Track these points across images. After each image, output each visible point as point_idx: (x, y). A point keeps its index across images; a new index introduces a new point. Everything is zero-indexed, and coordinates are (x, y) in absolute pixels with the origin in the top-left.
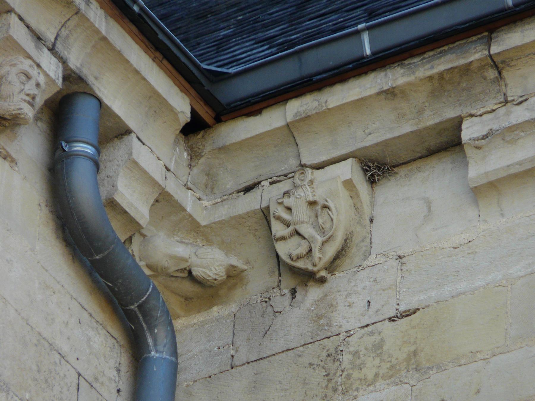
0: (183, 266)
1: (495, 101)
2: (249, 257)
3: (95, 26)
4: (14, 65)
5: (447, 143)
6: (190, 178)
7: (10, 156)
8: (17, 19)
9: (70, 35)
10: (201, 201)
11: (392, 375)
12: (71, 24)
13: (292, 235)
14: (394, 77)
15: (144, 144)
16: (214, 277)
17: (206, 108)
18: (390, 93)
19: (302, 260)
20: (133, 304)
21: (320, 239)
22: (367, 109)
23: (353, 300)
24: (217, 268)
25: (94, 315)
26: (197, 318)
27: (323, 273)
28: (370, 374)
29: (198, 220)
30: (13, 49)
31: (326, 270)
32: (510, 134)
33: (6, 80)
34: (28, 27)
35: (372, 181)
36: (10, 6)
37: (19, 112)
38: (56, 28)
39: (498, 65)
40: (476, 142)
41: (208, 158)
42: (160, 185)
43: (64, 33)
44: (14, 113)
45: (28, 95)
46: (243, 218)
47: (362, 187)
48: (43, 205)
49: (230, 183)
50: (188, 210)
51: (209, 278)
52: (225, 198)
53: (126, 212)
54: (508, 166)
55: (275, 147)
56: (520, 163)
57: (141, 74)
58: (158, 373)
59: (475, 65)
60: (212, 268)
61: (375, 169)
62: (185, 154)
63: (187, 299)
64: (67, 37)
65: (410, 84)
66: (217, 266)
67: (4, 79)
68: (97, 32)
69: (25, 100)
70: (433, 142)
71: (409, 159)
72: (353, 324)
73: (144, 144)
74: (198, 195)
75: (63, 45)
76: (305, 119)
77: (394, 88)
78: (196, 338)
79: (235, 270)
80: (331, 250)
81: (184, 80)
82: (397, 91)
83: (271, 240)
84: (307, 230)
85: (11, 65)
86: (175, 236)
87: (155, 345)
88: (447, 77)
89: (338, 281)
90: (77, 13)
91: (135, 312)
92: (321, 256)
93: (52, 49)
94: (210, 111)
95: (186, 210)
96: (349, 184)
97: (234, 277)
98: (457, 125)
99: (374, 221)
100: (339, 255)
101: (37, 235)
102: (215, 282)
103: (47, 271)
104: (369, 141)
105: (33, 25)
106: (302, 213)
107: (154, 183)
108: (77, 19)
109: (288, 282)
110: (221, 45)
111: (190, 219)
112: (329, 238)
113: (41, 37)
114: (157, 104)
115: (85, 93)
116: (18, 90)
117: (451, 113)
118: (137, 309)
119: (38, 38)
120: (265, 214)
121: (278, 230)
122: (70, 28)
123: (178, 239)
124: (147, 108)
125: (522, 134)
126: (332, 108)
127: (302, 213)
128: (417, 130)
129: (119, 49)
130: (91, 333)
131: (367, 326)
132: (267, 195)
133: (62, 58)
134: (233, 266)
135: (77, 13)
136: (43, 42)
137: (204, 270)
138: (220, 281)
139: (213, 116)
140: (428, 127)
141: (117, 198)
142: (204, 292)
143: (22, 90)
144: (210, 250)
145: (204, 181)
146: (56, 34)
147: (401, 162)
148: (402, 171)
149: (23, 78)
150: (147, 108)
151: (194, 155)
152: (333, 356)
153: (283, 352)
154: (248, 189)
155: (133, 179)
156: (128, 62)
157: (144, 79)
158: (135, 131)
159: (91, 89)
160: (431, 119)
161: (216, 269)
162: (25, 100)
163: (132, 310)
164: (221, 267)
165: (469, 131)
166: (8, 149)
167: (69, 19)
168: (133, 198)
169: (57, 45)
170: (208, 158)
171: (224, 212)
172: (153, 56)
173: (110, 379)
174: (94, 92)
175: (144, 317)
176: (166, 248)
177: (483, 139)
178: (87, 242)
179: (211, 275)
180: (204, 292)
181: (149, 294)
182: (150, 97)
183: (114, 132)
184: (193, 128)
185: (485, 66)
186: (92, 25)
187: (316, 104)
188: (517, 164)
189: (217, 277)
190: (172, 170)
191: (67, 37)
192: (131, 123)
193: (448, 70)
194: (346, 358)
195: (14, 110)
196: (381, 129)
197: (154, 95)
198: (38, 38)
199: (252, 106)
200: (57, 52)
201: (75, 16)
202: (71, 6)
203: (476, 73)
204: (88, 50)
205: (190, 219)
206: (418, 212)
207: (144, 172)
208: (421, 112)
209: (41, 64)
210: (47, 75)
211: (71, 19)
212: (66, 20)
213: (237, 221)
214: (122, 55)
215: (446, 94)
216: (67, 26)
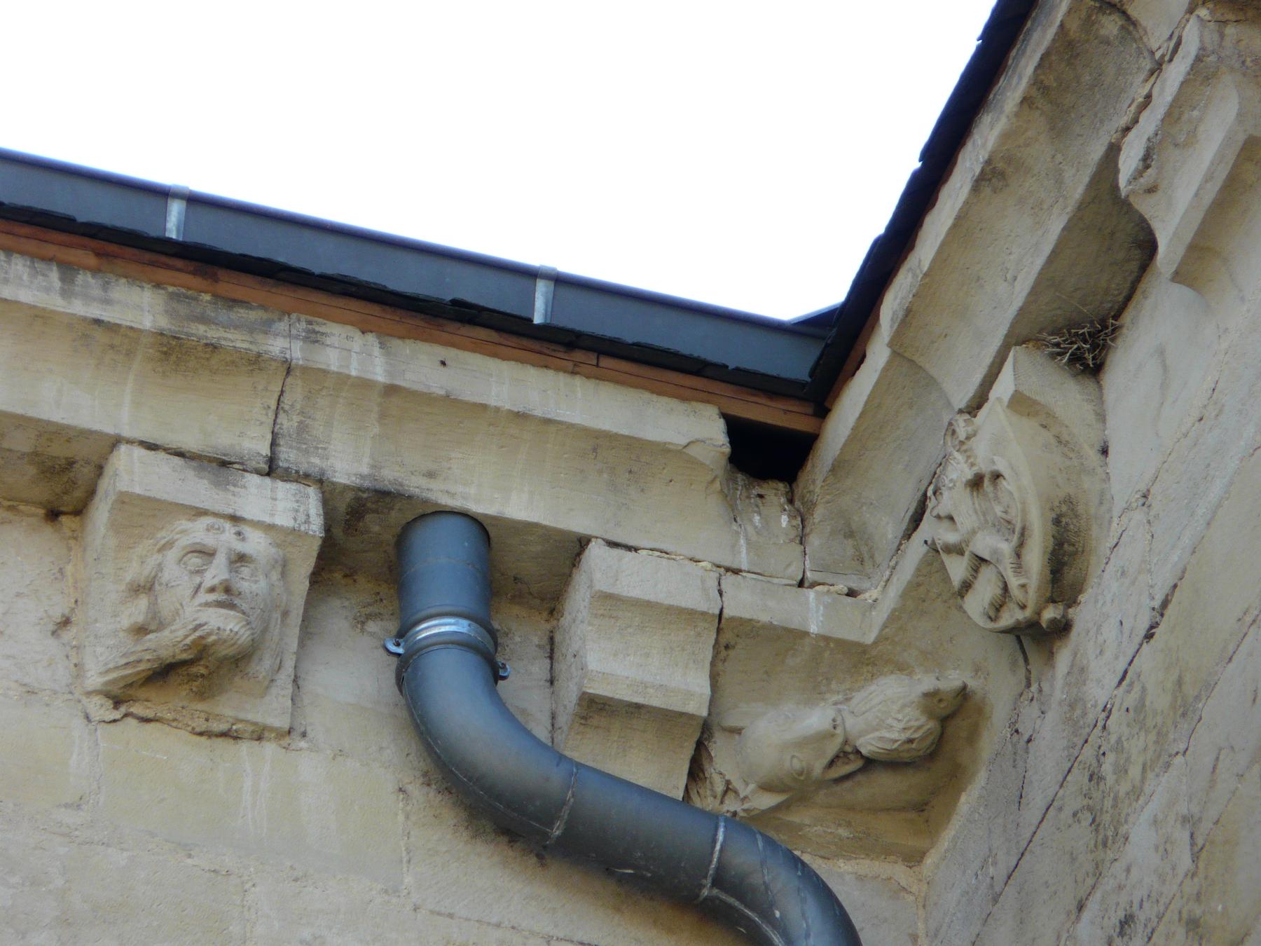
0: (832, 749)
1: (1142, 76)
3: (349, 377)
4: (169, 545)
6: (807, 562)
7: (265, 728)
8: (139, 452)
9: (308, 421)
10: (861, 597)
12: (295, 395)
13: (976, 570)
15: (636, 550)
16: (904, 737)
18: (990, 177)
19: (1005, 608)
20: (701, 887)
21: (1006, 548)
24: (900, 716)
27: (1050, 613)
30: (154, 516)
31: (1054, 602)
33: (161, 584)
34: (180, 454)
37: (198, 634)
38: (262, 423)
40: (1142, 180)
41: (828, 502)
42: (703, 614)
43: (288, 423)
44: (188, 641)
45: (212, 590)
46: (919, 585)
49: (888, 527)
50: (814, 629)
51: (896, 745)
52: (892, 563)
53: (638, 707)
54: (1196, 195)
55: (911, 407)
56: (1209, 178)
57: (534, 417)
59: (1074, 26)
60: (890, 721)
61: (1072, 343)
63: (921, 807)
64: (302, 428)
65: (1006, 136)
66: (899, 712)
67: (156, 585)
68: (364, 384)
69: (207, 604)
71: (1128, 285)
73: (636, 550)
75: (298, 449)
77: (989, 162)
79: (940, 701)
80: (1035, 558)
81: (681, 375)
82: (1000, 165)
84: (985, 543)
85: (159, 551)
86: (828, 696)
88: (1050, 80)
90: (289, 371)
91: (718, 898)
92: (1023, 581)
93: (272, 469)
94: (793, 406)
95: (806, 634)
97: (954, 716)
99: (1111, 451)
101: (404, 854)
102: (914, 746)
103: (451, 916)
105: (190, 442)
107: (689, 616)
108: (299, 382)
111: (832, 645)
112: (1022, 534)
113: (226, 458)
114: (625, 458)
115: (423, 516)
116: (189, 592)
118: (715, 891)
119: (221, 465)
122: (298, 406)
123: (835, 698)
124: (605, 476)
125: (1195, 113)
126: (930, 269)
128: (1070, 220)
129: (442, 392)
131: (1126, 672)
133: (307, 476)
134: (927, 695)
135: (289, 371)
136: (237, 466)
137: (877, 734)
138: (923, 738)
139: (810, 410)
140: (1081, 203)
143: (200, 586)
144: (873, 688)
145: (850, 551)
146: (269, 437)
147: (1121, 298)
148: (1127, 317)
149: (195, 561)
150: (605, 476)
155: (630, 630)
157: (548, 421)
158: (594, 534)
159: (426, 502)
161: (899, 721)
162: (207, 604)
163: (706, 899)
164: (907, 710)
166: (250, 717)
167: (282, 392)
169: (282, 456)
170: (828, 502)
172: (570, 365)
174: (437, 504)
175: (741, 899)
177: (1147, 167)
179: (895, 736)
181: (721, 850)
182: (595, 450)
183: (522, 579)
185: (1089, 16)
186: (343, 380)
187: (909, 279)
188: (1206, 181)
189: (908, 735)
190: (744, 566)
191: (302, 428)
192: (578, 524)
193: (1036, 69)
195: (186, 636)
197: (599, 444)
198: (221, 465)
200: (287, 469)
201: (289, 380)
202: (263, 365)
203: (1087, 41)
204: (376, 429)
205: (832, 645)
209: (238, 514)
210: (269, 528)
211: (287, 388)
212: (276, 396)
215: (1073, 115)
216: (287, 407)
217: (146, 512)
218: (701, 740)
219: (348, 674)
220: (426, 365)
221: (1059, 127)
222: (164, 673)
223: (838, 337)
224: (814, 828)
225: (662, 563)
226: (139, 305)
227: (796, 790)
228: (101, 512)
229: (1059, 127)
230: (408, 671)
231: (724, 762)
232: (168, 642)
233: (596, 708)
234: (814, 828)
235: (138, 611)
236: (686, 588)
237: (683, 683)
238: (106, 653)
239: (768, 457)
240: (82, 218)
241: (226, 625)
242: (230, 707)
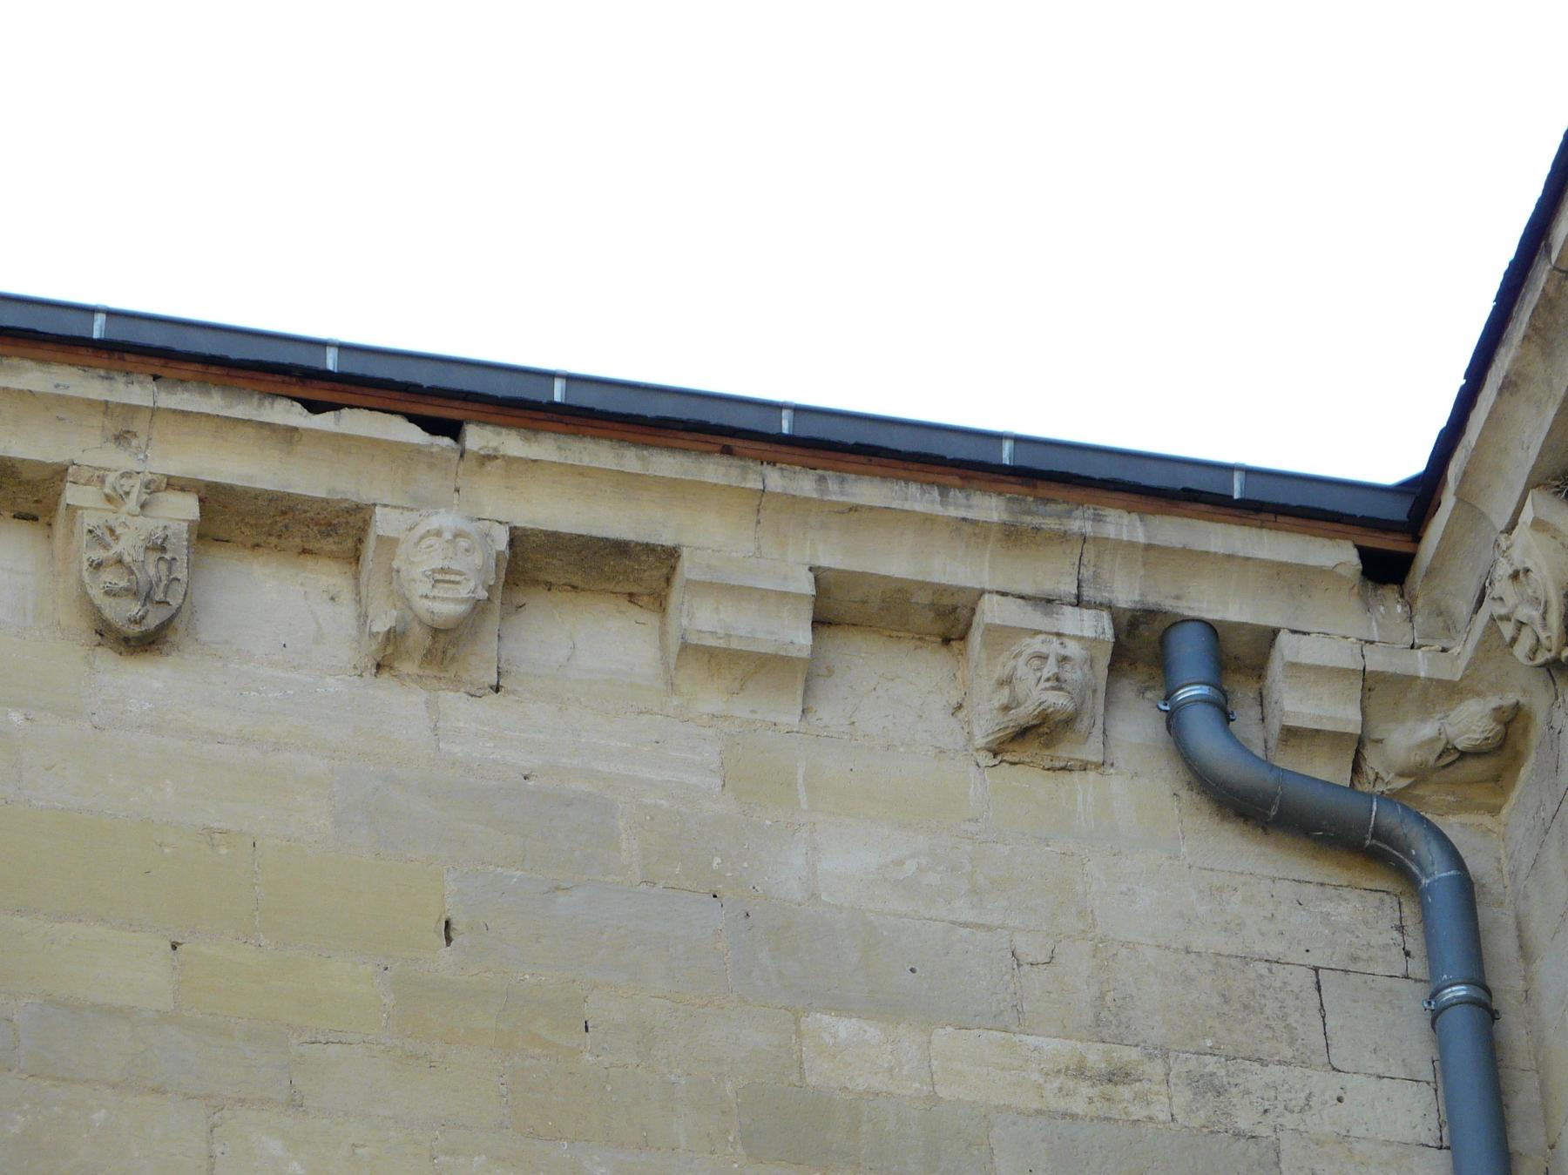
0: (1439, 747)
7: (1087, 763)
8: (996, 598)
12: (1090, 555)
17: (1391, 536)
21: (1536, 614)
25: (1326, 881)
29: (1447, 677)
34: (1022, 597)
36: (974, 589)
48: (1184, 793)
49: (1463, 607)
50: (1422, 674)
59: (1551, 290)
62: (1399, 608)
63: (1496, 779)
64: (1096, 575)
65: (1516, 360)
74: (1438, 647)
77: (1506, 377)
78: (1491, 841)
87: (1422, 869)
88: (1539, 324)
90: (1085, 541)
97: (1512, 722)
104: (1528, 468)
105: (1028, 589)
107: (1344, 673)
114: (1298, 578)
116: (1034, 682)
119: (1047, 602)
130: (1328, 907)
134: (1498, 709)
135: (1085, 541)
141: (1292, 722)
145: (1442, 625)
149: (1036, 662)
156: (1207, 553)
159: (1176, 614)
163: (1372, 846)
173: (1386, 947)
175: (1390, 843)
183: (1239, 658)
191: (1096, 575)
192: (1271, 621)
197: (1280, 569)
198: (1047, 602)
204: (1142, 572)
207: (1317, 669)
208: (1549, 383)
214: (1190, 551)
217: (1003, 635)
218: (1358, 748)
219: (1136, 725)
220: (1173, 530)
222: (1022, 734)
223: (1422, 493)
224: (1432, 799)
225: (1325, 643)
226: (989, 507)
227: (1418, 775)
228: (976, 637)
230: (1173, 720)
231: (1374, 761)
232: (1024, 714)
233: (1292, 735)
234: (1432, 799)
235: (1003, 696)
236: (1340, 655)
237: (1338, 711)
239: (1386, 569)
241: (1058, 701)
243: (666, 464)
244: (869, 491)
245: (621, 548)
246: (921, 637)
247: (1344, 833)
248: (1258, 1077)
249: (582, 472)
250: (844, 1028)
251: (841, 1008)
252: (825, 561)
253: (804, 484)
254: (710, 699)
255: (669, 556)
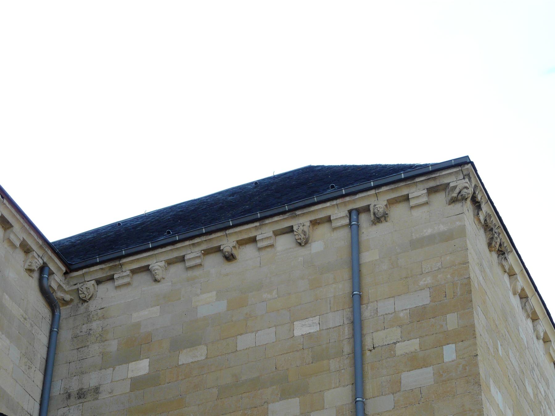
2: (74, 297)
5: (111, 278)
11: (99, 319)
14: (103, 266)
18: (102, 269)
22: (97, 271)
23: (93, 305)
26: (65, 307)
28: (95, 319)
32: (123, 277)
35: (98, 284)
39: (121, 265)
47: (96, 285)
49: (72, 283)
58: (57, 317)
70: (109, 278)
72: (93, 310)
76: (86, 273)
78: (64, 311)
80: (90, 296)
83: (79, 294)
84: (85, 292)
89: (90, 302)
96: (93, 285)
97: (72, 300)
98: (113, 275)
100: (91, 297)
104: (98, 277)
106: (84, 289)
109: (81, 302)
110: (72, 259)
117: (112, 273)
119: (39, 256)
120: (78, 289)
121: (80, 292)
127: (84, 289)
132: (78, 286)
142: (66, 303)
151: (66, 278)
152: (89, 315)
153: (357, 324)
154: (75, 285)
160: (109, 274)
165: (115, 277)
168: (54, 285)
171: (71, 289)
176: (60, 294)
178: (46, 294)
180: (66, 303)
183: (51, 273)
184: (66, 273)
194: (91, 316)
196: (100, 275)
198: (39, 256)
199: (77, 270)
206: (106, 289)
207: (56, 281)
213: (72, 290)
217: (34, 257)
221: (110, 270)
228: (30, 255)
229: (110, 270)
232: (31, 268)
235: (30, 264)
238: (26, 266)
240: (495, 204)
242: (31, 274)
243: (18, 217)
244: (32, 233)
245: (8, 222)
246: (23, 250)
247: (52, 303)
248: (36, 327)
249: (11, 212)
250: (7, 297)
251: (7, 294)
252: (25, 238)
253: (28, 227)
254: (6, 245)
255: (12, 226)
